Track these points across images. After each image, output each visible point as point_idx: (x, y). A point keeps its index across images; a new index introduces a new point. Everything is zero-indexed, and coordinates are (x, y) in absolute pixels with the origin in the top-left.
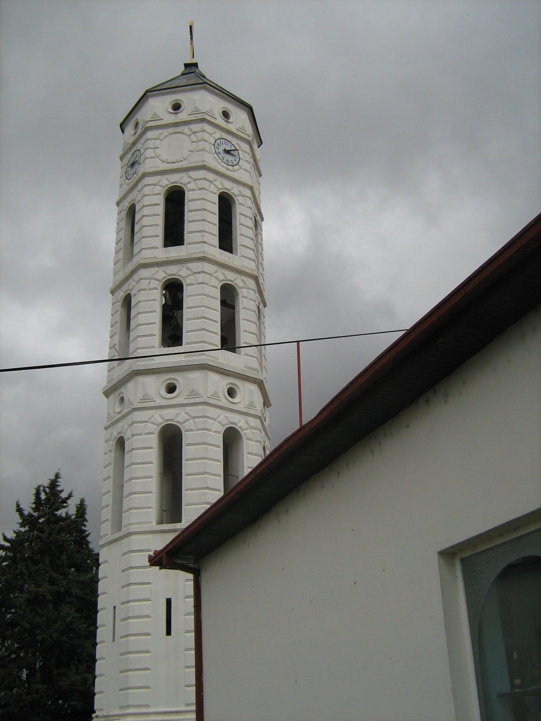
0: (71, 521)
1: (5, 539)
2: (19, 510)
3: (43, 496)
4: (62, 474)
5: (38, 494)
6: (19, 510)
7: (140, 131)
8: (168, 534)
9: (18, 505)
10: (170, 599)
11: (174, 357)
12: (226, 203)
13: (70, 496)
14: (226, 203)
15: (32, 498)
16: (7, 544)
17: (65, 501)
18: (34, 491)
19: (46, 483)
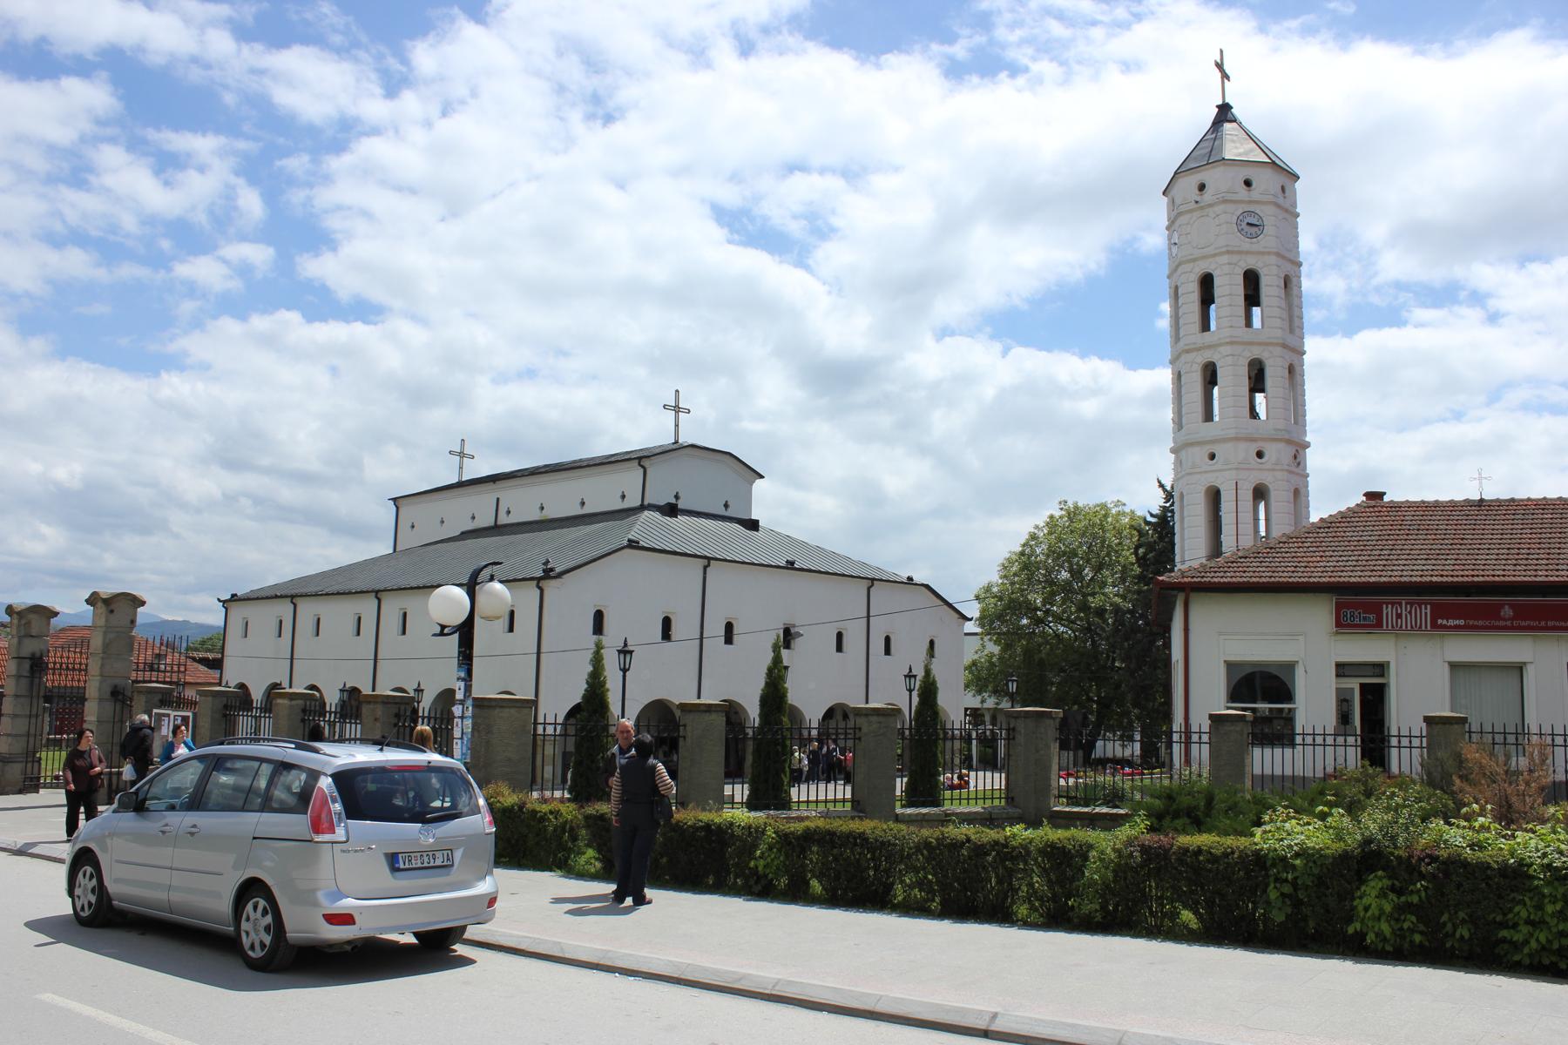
2: (1161, 486)
6: (1161, 486)
10: (1339, 666)
11: (1208, 430)
16: (1153, 520)
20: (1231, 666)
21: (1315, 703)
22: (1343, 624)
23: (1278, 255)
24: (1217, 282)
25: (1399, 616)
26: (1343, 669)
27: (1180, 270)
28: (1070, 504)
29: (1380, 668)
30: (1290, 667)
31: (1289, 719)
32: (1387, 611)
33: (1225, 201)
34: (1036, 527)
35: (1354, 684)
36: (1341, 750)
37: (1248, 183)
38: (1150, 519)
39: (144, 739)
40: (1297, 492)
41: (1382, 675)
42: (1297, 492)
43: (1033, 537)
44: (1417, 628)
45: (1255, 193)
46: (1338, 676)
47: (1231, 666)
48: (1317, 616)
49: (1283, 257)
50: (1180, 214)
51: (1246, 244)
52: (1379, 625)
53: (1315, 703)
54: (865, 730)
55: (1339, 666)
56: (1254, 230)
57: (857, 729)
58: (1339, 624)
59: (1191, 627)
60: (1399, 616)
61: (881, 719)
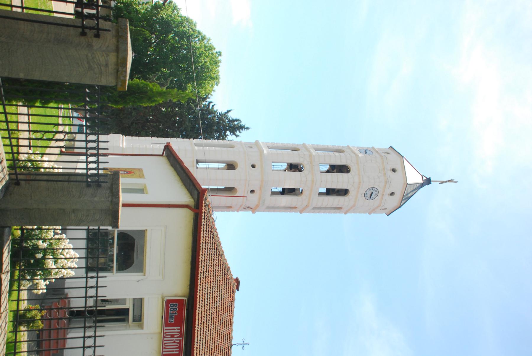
0: (28, 326)
1: (213, 106)
2: (228, 111)
3: (236, 123)
4: (249, 130)
5: (237, 120)
6: (228, 111)
7: (383, 154)
8: (43, 21)
9: (230, 111)
10: (141, 300)
12: (344, 192)
13: (237, 136)
14: (344, 192)
15: (234, 118)
16: (211, 107)
17: (234, 134)
18: (238, 118)
19: (243, 124)
20: (142, 233)
21: (116, 286)
22: (169, 303)
23: (354, 205)
24: (345, 175)
25: (172, 336)
26: (139, 303)
27: (353, 155)
28: (220, 58)
29: (139, 319)
30: (141, 269)
31: (107, 268)
32: (176, 330)
33: (386, 182)
34: (209, 40)
35: (129, 305)
36: (82, 292)
37: (392, 194)
38: (211, 105)
39: (109, 270)
40: (230, 207)
41: (134, 321)
42: (230, 207)
43: (203, 38)
44: (164, 346)
45: (387, 197)
46: (134, 299)
47: (142, 233)
48: (178, 288)
49: (352, 207)
50: (382, 157)
51: (362, 191)
52: (167, 324)
53: (116, 286)
54: (97, 43)
55: (141, 300)
56: (369, 196)
57: (98, 33)
58: (169, 302)
59: (171, 209)
60: (172, 336)
61: (112, 67)
